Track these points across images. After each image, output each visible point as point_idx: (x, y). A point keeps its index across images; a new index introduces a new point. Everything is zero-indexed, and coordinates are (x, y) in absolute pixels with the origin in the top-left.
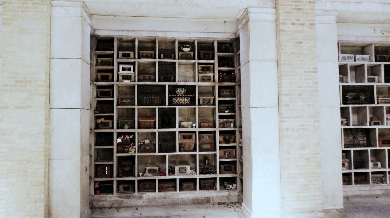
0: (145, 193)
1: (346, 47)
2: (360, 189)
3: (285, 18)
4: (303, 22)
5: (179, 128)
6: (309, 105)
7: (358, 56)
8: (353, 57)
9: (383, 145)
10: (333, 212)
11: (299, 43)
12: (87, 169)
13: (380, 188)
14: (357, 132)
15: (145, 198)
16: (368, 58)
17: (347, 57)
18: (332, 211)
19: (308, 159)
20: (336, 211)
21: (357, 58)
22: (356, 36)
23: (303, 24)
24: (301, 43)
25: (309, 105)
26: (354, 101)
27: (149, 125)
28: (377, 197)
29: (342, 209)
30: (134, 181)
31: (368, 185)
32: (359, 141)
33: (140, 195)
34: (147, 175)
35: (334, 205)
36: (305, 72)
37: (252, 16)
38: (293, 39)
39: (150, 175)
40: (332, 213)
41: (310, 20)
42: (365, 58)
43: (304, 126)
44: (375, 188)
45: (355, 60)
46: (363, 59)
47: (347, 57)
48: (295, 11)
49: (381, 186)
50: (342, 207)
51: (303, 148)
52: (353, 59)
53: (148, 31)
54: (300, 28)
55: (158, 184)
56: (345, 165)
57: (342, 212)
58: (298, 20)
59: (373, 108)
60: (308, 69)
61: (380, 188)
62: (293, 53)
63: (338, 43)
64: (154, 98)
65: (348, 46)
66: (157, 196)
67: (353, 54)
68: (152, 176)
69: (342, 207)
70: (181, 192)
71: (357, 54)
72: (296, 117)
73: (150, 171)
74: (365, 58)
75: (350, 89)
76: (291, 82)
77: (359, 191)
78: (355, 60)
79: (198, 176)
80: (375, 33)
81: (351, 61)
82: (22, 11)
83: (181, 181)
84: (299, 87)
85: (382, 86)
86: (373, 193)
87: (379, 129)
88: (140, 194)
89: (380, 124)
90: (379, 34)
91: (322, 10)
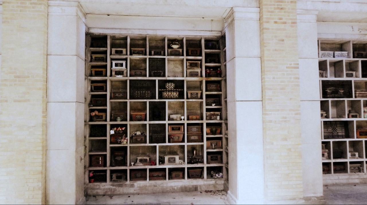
0: (137, 182)
1: (326, 44)
2: (339, 178)
3: (268, 17)
4: (285, 21)
5: (169, 120)
6: (291, 99)
7: (337, 53)
8: (332, 54)
9: (360, 136)
10: (313, 199)
11: (281, 41)
12: (81, 159)
13: (357, 177)
14: (336, 124)
15: (136, 186)
16: (347, 55)
17: (326, 54)
18: (313, 198)
19: (290, 150)
20: (316, 199)
21: (336, 55)
22: (335, 34)
23: (285, 23)
24: (283, 40)
25: (291, 99)
26: (333, 95)
27: (140, 117)
28: (355, 185)
29: (321, 196)
30: (126, 170)
31: (346, 174)
32: (337, 132)
33: (132, 183)
34: (138, 164)
35: (314, 193)
36: (287, 68)
37: (237, 15)
38: (276, 37)
39: (141, 164)
40: (313, 200)
41: (291, 19)
42: (343, 54)
43: (286, 119)
44: (353, 177)
45: (334, 57)
46: (342, 56)
47: (326, 54)
48: (278, 10)
49: (358, 175)
50: (322, 195)
51: (285, 139)
52: (333, 56)
53: (139, 29)
54: (282, 26)
55: (149, 173)
56: (325, 156)
57: (322, 199)
58: (281, 19)
59: (351, 101)
60: (290, 65)
61: (357, 177)
62: (276, 50)
63: (318, 41)
64: (145, 92)
65: (327, 44)
66: (148, 185)
67: (333, 51)
68: (143, 166)
69: (322, 195)
70: (171, 181)
71: (336, 51)
72: (278, 110)
73: (141, 161)
74: (343, 54)
75: (330, 83)
76: (274, 77)
77: (337, 179)
78: (334, 57)
79: (186, 166)
80: (353, 31)
81: (331, 58)
82: (21, 11)
83: (171, 170)
84: (281, 82)
85: (360, 81)
86: (351, 181)
87: (357, 122)
88: (132, 182)
89: (358, 117)
90: (356, 32)
91: (303, 10)
